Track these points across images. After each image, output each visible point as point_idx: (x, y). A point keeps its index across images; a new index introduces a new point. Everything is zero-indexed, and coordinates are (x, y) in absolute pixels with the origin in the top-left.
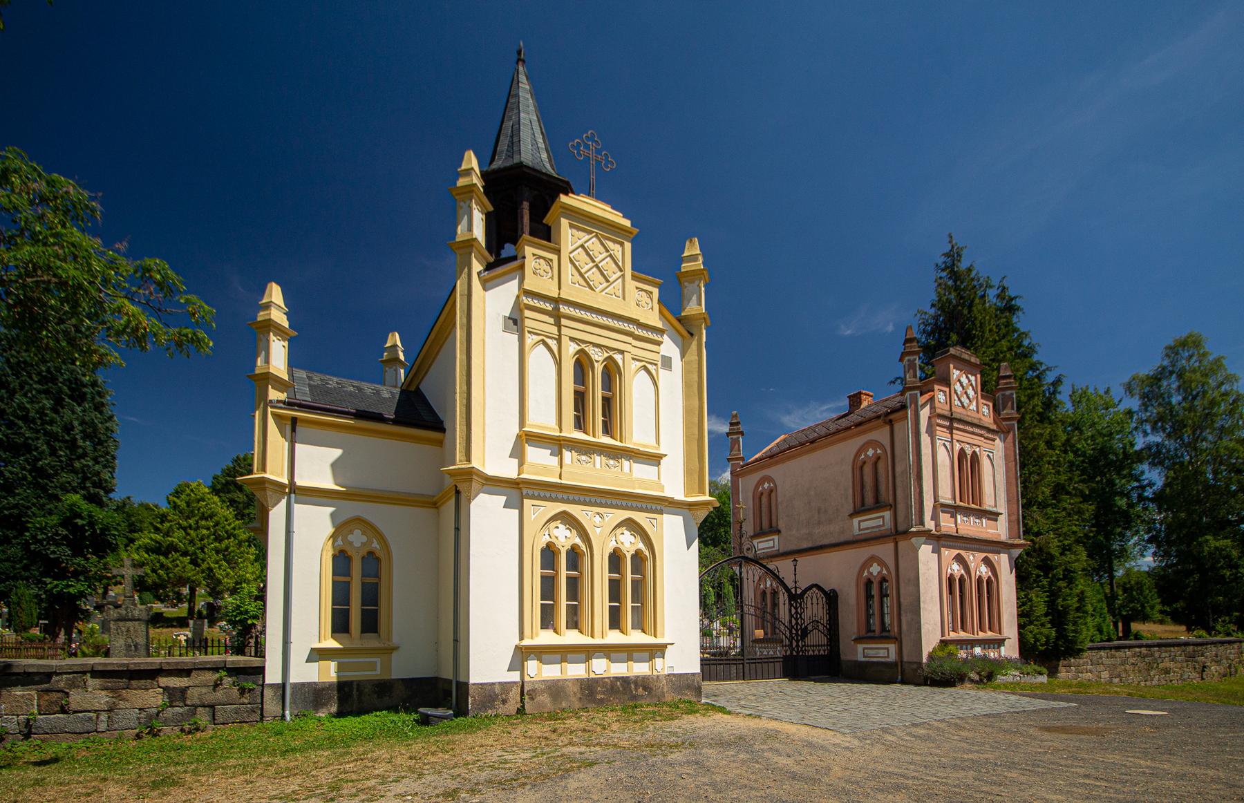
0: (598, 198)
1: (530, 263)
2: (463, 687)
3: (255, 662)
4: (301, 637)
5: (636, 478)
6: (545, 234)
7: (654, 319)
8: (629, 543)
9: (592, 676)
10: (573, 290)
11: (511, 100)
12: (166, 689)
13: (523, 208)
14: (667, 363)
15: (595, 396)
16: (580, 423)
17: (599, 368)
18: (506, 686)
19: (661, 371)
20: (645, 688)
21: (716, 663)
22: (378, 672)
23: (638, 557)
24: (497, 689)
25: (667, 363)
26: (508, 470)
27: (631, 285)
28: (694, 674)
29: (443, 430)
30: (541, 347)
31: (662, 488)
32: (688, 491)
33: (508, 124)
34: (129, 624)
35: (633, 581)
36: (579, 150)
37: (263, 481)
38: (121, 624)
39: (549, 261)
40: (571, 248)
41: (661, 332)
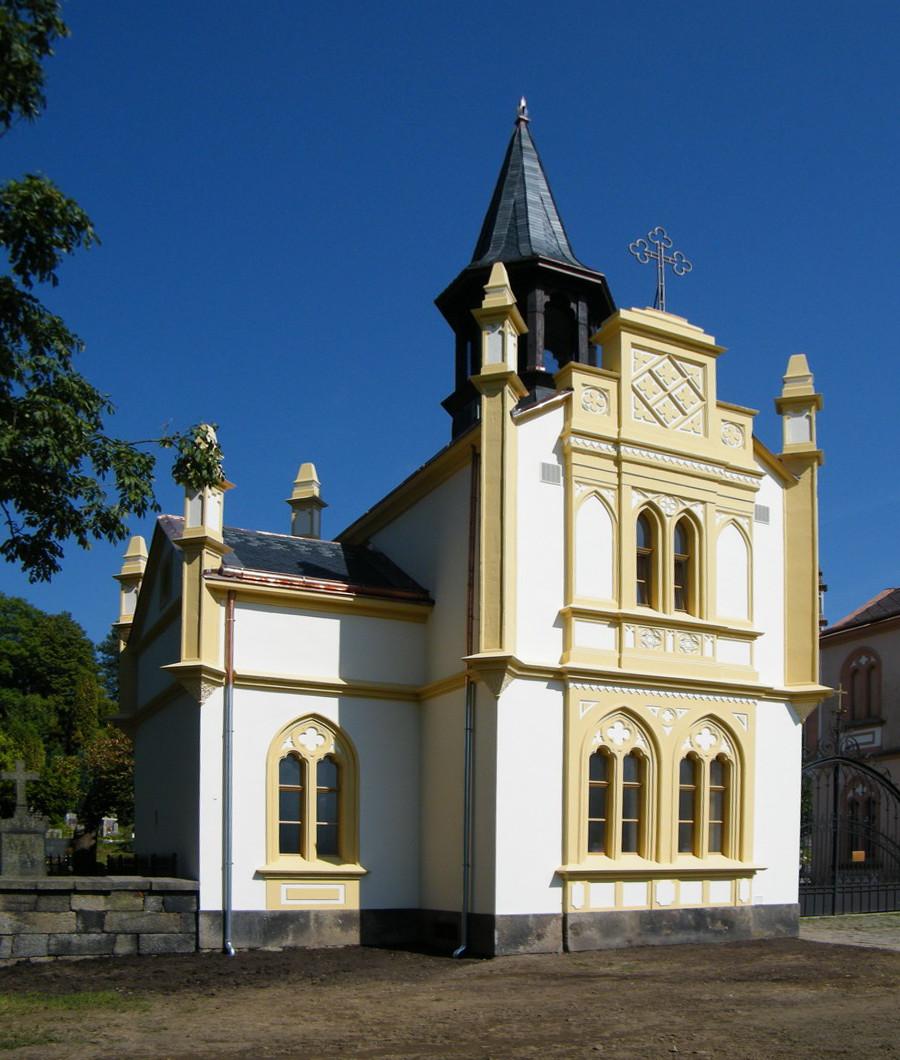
0: (671, 310)
1: (579, 395)
2: (488, 921)
3: (185, 884)
4: (245, 859)
5: (724, 660)
6: (606, 361)
7: (746, 458)
8: (709, 745)
9: (656, 907)
10: (638, 427)
11: (511, 172)
12: (80, 913)
13: (572, 323)
14: (763, 514)
15: (666, 562)
16: (646, 595)
17: (671, 524)
18: (542, 920)
19: (756, 525)
20: (725, 922)
21: (826, 877)
22: (341, 901)
23: (721, 765)
24: (531, 923)
25: (763, 514)
26: (549, 656)
27: (717, 414)
28: (789, 906)
29: (432, 603)
30: (594, 500)
31: (756, 675)
32: (789, 679)
33: (507, 203)
34: (24, 837)
35: (712, 792)
36: (680, 262)
37: (198, 669)
38: (15, 837)
39: (603, 392)
40: (634, 374)
41: (759, 475)
